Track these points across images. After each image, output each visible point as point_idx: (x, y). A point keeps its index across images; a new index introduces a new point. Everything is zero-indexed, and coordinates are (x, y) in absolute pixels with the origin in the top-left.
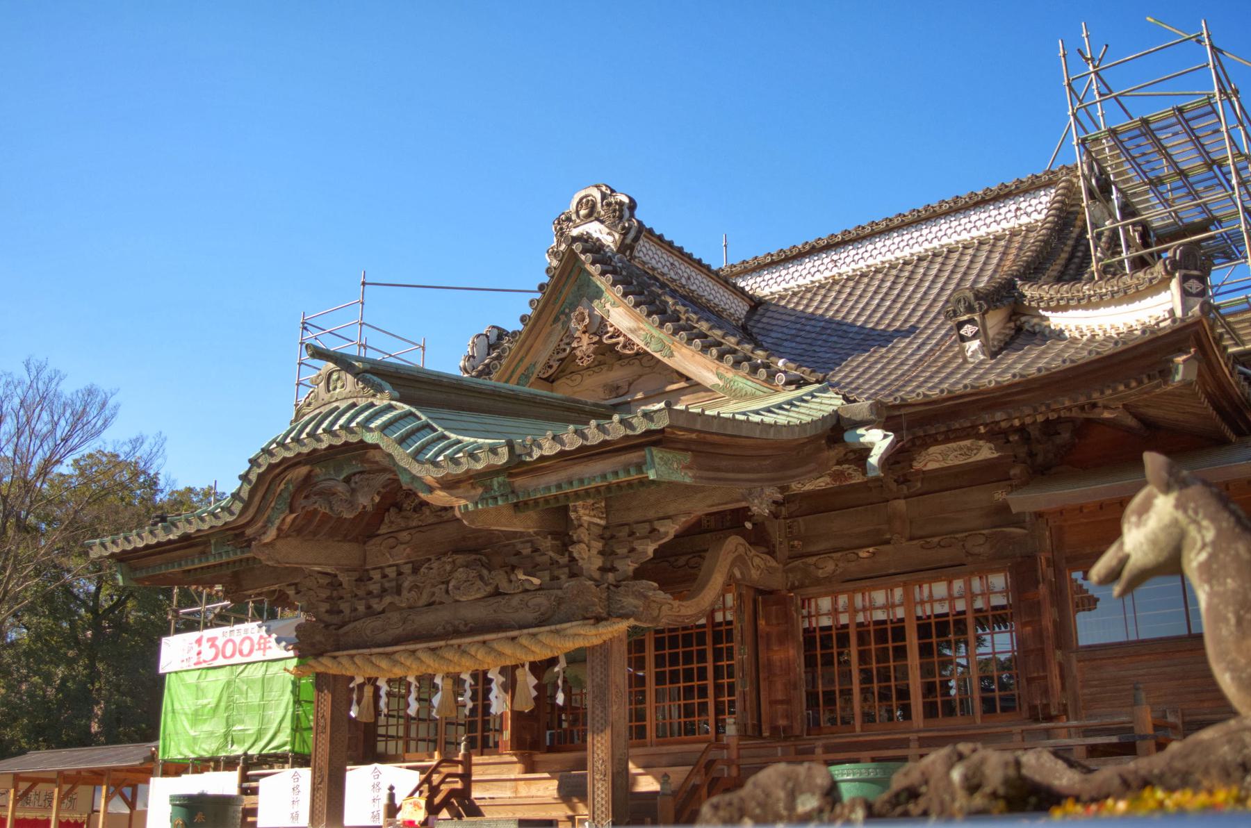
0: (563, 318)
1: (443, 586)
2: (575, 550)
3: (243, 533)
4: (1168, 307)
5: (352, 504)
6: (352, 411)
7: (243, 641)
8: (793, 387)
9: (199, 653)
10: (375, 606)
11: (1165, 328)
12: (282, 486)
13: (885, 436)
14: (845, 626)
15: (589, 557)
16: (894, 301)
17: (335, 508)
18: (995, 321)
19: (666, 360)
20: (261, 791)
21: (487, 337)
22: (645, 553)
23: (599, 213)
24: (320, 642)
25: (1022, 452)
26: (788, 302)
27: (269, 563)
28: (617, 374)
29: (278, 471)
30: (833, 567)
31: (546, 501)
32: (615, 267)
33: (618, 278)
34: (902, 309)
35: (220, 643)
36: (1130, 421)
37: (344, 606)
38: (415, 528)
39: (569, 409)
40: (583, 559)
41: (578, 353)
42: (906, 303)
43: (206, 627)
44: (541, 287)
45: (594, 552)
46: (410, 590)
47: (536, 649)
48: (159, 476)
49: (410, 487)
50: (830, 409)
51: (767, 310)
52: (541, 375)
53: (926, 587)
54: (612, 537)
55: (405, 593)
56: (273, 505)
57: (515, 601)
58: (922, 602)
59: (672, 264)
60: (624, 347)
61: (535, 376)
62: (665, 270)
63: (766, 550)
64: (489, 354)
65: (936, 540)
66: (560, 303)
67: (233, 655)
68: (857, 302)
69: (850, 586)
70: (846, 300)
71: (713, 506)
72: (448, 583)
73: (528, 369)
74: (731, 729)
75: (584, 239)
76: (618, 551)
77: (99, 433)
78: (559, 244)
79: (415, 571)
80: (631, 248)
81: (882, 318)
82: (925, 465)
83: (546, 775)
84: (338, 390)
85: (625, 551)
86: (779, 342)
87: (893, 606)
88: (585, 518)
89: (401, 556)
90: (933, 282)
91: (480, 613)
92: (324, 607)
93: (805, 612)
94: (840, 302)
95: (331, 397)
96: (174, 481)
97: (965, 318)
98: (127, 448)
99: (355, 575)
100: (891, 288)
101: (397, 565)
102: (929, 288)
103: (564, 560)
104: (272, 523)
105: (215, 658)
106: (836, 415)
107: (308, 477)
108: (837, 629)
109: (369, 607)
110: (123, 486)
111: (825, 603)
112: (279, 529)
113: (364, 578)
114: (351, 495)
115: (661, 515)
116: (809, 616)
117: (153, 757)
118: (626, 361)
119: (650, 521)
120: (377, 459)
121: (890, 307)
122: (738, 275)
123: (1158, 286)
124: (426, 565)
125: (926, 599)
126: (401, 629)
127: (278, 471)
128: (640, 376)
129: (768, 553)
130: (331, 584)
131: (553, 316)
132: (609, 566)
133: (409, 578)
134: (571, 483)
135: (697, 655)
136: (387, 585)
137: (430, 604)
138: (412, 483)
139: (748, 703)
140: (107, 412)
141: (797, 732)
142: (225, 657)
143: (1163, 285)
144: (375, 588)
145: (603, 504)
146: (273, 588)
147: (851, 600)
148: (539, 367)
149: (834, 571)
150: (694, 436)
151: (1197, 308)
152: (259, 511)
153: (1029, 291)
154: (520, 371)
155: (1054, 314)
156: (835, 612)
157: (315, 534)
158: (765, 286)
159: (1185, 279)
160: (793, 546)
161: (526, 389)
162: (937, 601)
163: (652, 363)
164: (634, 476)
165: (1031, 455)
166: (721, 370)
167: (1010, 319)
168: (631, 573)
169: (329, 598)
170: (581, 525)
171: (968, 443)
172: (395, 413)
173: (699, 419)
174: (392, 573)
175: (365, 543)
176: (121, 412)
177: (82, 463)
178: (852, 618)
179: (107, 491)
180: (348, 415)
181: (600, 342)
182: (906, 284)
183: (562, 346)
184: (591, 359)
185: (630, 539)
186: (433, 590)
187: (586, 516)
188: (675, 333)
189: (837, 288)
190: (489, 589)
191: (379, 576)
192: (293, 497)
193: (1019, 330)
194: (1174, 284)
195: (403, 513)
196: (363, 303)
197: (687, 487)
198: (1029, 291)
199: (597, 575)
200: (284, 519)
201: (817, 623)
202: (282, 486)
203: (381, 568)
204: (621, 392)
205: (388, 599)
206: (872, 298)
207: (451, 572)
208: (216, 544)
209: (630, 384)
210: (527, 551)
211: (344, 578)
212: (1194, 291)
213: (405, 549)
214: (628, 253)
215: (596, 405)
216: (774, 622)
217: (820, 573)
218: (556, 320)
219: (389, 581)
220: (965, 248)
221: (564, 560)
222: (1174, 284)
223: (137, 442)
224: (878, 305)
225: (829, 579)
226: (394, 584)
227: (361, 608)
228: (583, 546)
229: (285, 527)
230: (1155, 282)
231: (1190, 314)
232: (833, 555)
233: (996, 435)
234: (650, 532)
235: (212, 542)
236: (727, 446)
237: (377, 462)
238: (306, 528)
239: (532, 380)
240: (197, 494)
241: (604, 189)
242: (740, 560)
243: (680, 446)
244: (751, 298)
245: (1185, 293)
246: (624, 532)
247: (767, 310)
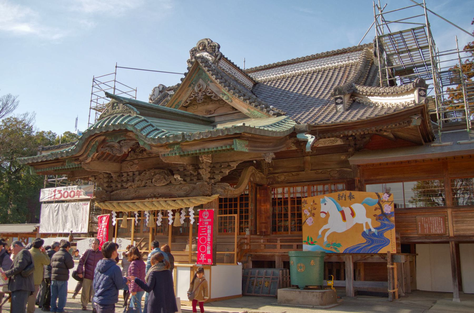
0: (192, 85)
1: (150, 180)
2: (201, 171)
3: (78, 159)
4: (413, 99)
5: (121, 151)
6: (122, 118)
7: (71, 192)
8: (276, 116)
9: (55, 195)
10: (124, 186)
11: (411, 107)
12: (94, 143)
13: (312, 137)
14: (287, 198)
15: (206, 174)
16: (306, 86)
17: (114, 152)
18: (346, 98)
19: (229, 103)
20: (78, 244)
21: (159, 88)
22: (225, 173)
23: (207, 49)
24: (104, 197)
25: (352, 143)
26: (267, 83)
27: (88, 170)
28: (210, 107)
29: (93, 137)
30: (284, 178)
31: (192, 154)
32: (212, 69)
33: (213, 73)
34: (309, 89)
35: (62, 192)
36: (392, 136)
37: (113, 185)
38: (140, 159)
39: (195, 118)
40: (204, 174)
41: (197, 98)
42: (310, 87)
43: (58, 186)
44: (185, 74)
45: (207, 172)
46: (138, 181)
48: (33, 127)
49: (143, 146)
50: (293, 126)
51: (260, 86)
52: (183, 105)
53: (315, 187)
54: (214, 167)
55: (136, 182)
56: (90, 149)
57: (177, 187)
59: (230, 68)
60: (215, 97)
61: (181, 105)
62: (227, 70)
63: (260, 171)
64: (159, 94)
65: (320, 171)
66: (191, 80)
67: (67, 197)
68: (292, 85)
69: (289, 185)
70: (288, 85)
71: (251, 158)
72: (152, 179)
73: (179, 102)
74: (248, 232)
75: (202, 58)
76: (216, 172)
77: (12, 111)
78: (192, 59)
79: (140, 174)
80: (218, 62)
81: (287, 86)
82: (318, 145)
85: (218, 172)
86: (265, 98)
87: (304, 192)
88: (205, 160)
89: (135, 168)
90: (319, 81)
91: (164, 190)
92: (105, 185)
93: (273, 192)
94: (286, 85)
95: (114, 112)
96: (38, 129)
97: (338, 96)
98: (22, 117)
99: (118, 174)
100: (304, 82)
101: (133, 172)
102: (318, 83)
103: (196, 174)
104: (90, 156)
105: (61, 197)
106: (294, 128)
107: (104, 141)
108: (284, 199)
109: (122, 186)
110: (20, 129)
111: (280, 190)
112: (92, 158)
113: (121, 175)
114: (120, 148)
115: (232, 160)
116: (274, 194)
117: (37, 230)
118: (214, 102)
119: (228, 162)
120: (131, 135)
121: (305, 89)
122: (250, 73)
123: (408, 92)
124: (144, 172)
125: (315, 191)
126: (134, 194)
127: (93, 137)
128: (219, 108)
129: (261, 172)
130: (108, 177)
131: (189, 85)
132: (212, 177)
133: (138, 177)
134: (205, 149)
135: (234, 205)
136: (129, 178)
137: (145, 186)
138: (144, 145)
139: (253, 223)
140: (15, 104)
141: (269, 233)
142: (64, 197)
143: (412, 91)
144: (125, 179)
145: (211, 155)
146: (86, 177)
147: (289, 190)
148: (183, 102)
149: (284, 179)
150: (250, 135)
151: (424, 101)
152: (85, 152)
153: (360, 88)
154: (175, 104)
155: (373, 98)
156: (283, 193)
157: (104, 159)
158: (260, 77)
159: (420, 90)
160: (270, 170)
161: (177, 110)
163: (224, 103)
164: (228, 147)
165: (355, 144)
166: (249, 108)
167: (351, 97)
168: (220, 180)
169: (108, 182)
170: (203, 163)
171: (333, 139)
172: (139, 120)
173: (258, 130)
174: (131, 174)
175: (121, 163)
176: (20, 103)
177: (5, 121)
178: (289, 196)
179: (13, 132)
180: (121, 119)
181: (206, 95)
182: (310, 81)
183: (192, 95)
184: (202, 101)
185: (220, 168)
186: (146, 181)
187: (206, 160)
188: (234, 94)
189: (285, 80)
190: (168, 182)
191: (126, 175)
192: (98, 147)
193: (354, 101)
194: (416, 92)
195: (136, 153)
196: (116, 74)
197: (247, 153)
198: (360, 88)
199: (208, 180)
200: (94, 155)
201: (277, 196)
202: (94, 143)
203: (127, 172)
204: (212, 113)
205: (129, 184)
206: (298, 85)
207: (153, 176)
208: (68, 162)
209: (215, 110)
210: (182, 169)
211: (113, 175)
212: (422, 95)
213: (136, 166)
214: (216, 64)
215: (203, 117)
216: (262, 196)
217: (279, 180)
218: (190, 86)
219: (130, 177)
220: (330, 70)
221: (196, 174)
222: (416, 92)
223: (26, 114)
224: (300, 87)
225: (282, 182)
226: (132, 178)
227: (119, 186)
228: (204, 170)
229: (94, 157)
230: (409, 90)
231: (421, 103)
232: (284, 174)
233: (346, 138)
234: (228, 166)
235: (67, 161)
236: (260, 139)
237: (131, 137)
238: (101, 158)
239: (180, 107)
240: (46, 133)
241: (209, 40)
242: (253, 175)
243: (245, 139)
244: (254, 81)
245: (420, 95)
246: (218, 166)
247: (260, 86)
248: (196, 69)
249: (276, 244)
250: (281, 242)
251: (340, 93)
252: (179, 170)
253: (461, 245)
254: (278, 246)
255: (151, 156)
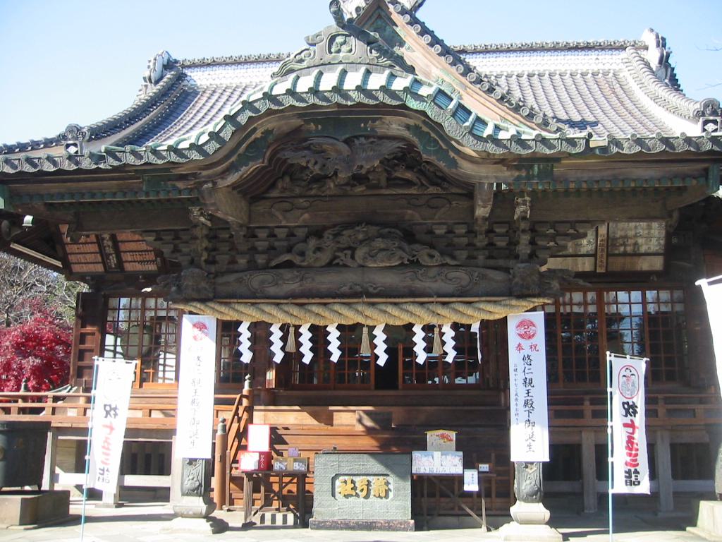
1: (349, 252)
47: (231, 313)
53: (568, 295)
54: (215, 249)
58: (609, 304)
83: (297, 408)
84: (341, 55)
97: (711, 118)
132: (211, 259)
162: (153, 309)
174: (282, 233)
213: (302, 214)
227: (242, 261)
248: (370, 17)
249: (580, 407)
250: (591, 404)
251: (714, 113)
252: (434, 233)
253: (152, 411)
254: (588, 413)
255: (350, 193)
